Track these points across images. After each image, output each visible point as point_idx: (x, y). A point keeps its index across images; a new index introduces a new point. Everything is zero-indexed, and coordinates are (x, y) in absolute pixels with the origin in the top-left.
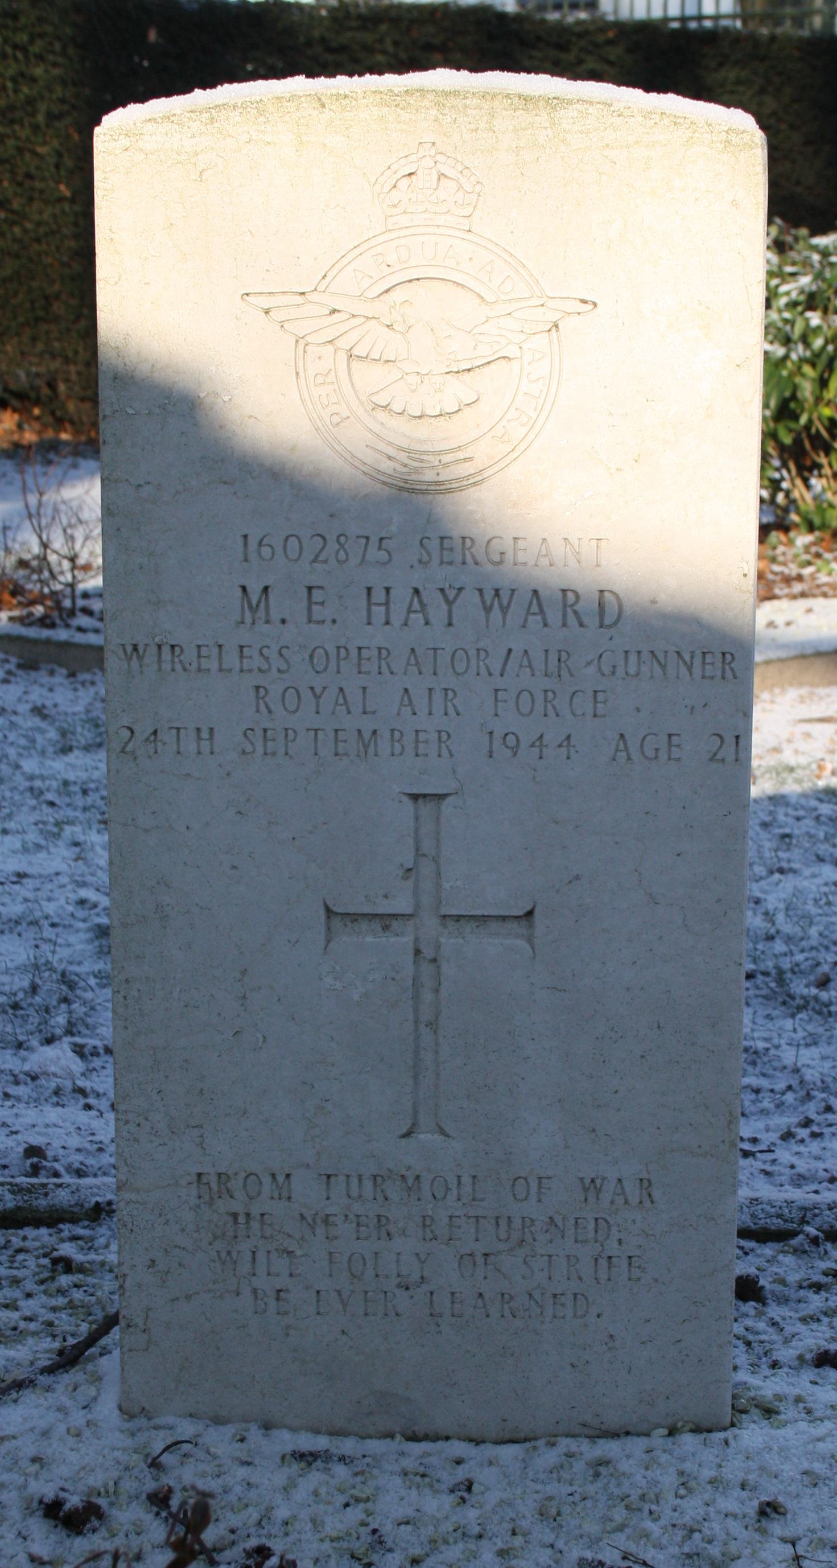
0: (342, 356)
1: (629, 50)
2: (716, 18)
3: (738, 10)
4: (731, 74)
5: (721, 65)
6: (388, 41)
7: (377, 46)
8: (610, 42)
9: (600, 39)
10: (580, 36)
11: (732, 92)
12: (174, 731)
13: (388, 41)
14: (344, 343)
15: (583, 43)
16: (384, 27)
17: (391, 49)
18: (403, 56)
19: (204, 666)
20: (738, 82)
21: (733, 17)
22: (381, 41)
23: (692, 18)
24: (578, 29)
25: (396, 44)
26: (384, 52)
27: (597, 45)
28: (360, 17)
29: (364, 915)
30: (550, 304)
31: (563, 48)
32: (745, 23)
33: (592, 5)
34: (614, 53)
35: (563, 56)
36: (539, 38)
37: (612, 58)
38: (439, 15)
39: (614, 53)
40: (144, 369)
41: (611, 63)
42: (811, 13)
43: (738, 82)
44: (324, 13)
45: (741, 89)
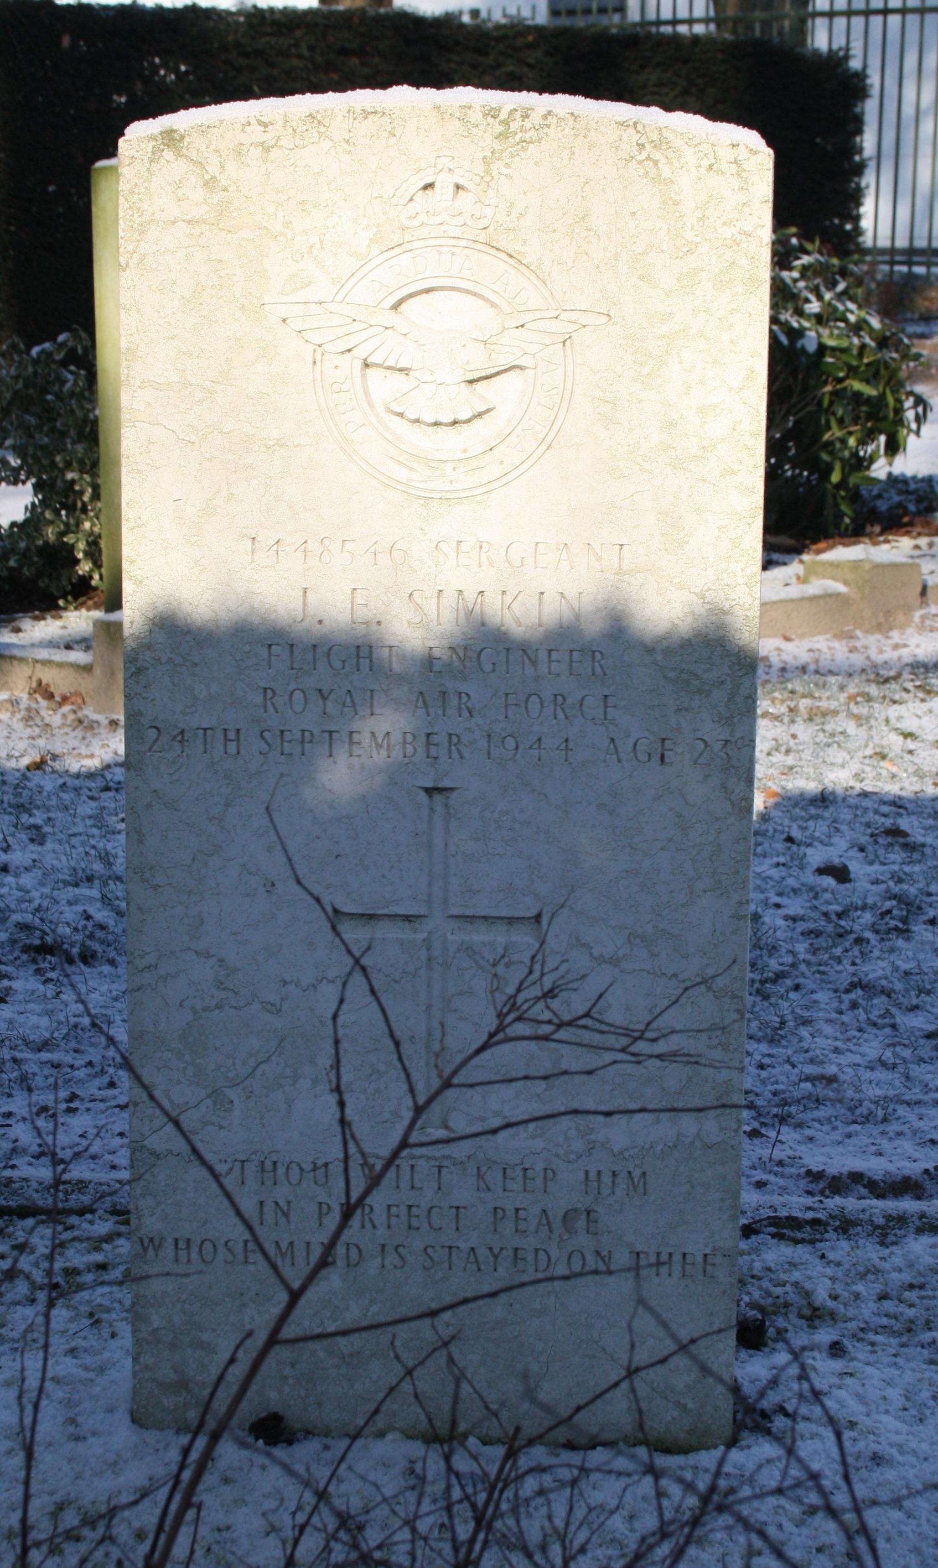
0: (358, 364)
1: (548, 54)
2: (674, 22)
3: (712, 13)
4: (653, 76)
5: (643, 67)
6: (304, 45)
7: (293, 50)
8: (530, 46)
9: (519, 43)
10: (498, 40)
11: (654, 93)
12: (454, 1210)
13: (304, 45)
14: (361, 352)
15: (501, 46)
16: (298, 33)
17: (305, 52)
18: (319, 59)
19: (509, 1187)
20: (660, 84)
21: (706, 21)
22: (296, 45)
23: (666, 23)
24: (495, 34)
25: (311, 48)
26: (300, 56)
27: (515, 49)
28: (275, 23)
29: (518, 918)
30: (565, 316)
31: (483, 52)
32: (718, 26)
33: (621, 9)
34: (534, 56)
35: (481, 59)
36: (457, 43)
37: (531, 61)
38: (356, 20)
39: (534, 56)
40: (256, 620)
41: (530, 66)
42: (780, 18)
43: (660, 84)
44: (242, 19)
45: (664, 90)
